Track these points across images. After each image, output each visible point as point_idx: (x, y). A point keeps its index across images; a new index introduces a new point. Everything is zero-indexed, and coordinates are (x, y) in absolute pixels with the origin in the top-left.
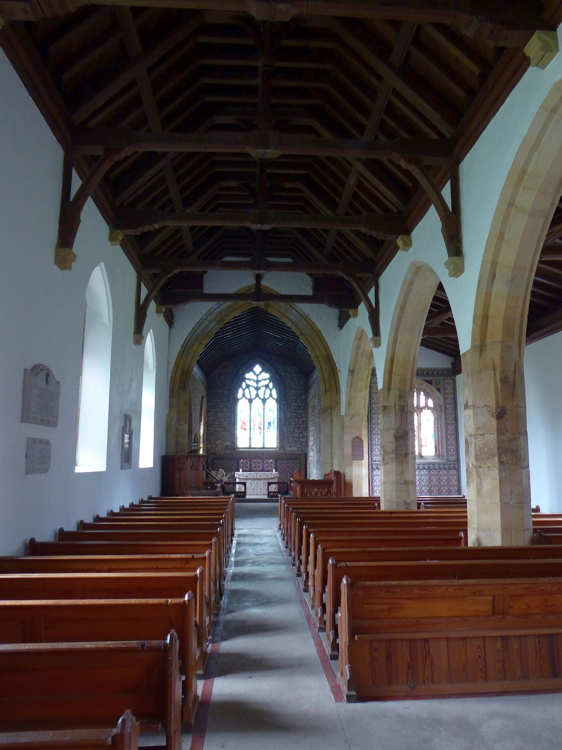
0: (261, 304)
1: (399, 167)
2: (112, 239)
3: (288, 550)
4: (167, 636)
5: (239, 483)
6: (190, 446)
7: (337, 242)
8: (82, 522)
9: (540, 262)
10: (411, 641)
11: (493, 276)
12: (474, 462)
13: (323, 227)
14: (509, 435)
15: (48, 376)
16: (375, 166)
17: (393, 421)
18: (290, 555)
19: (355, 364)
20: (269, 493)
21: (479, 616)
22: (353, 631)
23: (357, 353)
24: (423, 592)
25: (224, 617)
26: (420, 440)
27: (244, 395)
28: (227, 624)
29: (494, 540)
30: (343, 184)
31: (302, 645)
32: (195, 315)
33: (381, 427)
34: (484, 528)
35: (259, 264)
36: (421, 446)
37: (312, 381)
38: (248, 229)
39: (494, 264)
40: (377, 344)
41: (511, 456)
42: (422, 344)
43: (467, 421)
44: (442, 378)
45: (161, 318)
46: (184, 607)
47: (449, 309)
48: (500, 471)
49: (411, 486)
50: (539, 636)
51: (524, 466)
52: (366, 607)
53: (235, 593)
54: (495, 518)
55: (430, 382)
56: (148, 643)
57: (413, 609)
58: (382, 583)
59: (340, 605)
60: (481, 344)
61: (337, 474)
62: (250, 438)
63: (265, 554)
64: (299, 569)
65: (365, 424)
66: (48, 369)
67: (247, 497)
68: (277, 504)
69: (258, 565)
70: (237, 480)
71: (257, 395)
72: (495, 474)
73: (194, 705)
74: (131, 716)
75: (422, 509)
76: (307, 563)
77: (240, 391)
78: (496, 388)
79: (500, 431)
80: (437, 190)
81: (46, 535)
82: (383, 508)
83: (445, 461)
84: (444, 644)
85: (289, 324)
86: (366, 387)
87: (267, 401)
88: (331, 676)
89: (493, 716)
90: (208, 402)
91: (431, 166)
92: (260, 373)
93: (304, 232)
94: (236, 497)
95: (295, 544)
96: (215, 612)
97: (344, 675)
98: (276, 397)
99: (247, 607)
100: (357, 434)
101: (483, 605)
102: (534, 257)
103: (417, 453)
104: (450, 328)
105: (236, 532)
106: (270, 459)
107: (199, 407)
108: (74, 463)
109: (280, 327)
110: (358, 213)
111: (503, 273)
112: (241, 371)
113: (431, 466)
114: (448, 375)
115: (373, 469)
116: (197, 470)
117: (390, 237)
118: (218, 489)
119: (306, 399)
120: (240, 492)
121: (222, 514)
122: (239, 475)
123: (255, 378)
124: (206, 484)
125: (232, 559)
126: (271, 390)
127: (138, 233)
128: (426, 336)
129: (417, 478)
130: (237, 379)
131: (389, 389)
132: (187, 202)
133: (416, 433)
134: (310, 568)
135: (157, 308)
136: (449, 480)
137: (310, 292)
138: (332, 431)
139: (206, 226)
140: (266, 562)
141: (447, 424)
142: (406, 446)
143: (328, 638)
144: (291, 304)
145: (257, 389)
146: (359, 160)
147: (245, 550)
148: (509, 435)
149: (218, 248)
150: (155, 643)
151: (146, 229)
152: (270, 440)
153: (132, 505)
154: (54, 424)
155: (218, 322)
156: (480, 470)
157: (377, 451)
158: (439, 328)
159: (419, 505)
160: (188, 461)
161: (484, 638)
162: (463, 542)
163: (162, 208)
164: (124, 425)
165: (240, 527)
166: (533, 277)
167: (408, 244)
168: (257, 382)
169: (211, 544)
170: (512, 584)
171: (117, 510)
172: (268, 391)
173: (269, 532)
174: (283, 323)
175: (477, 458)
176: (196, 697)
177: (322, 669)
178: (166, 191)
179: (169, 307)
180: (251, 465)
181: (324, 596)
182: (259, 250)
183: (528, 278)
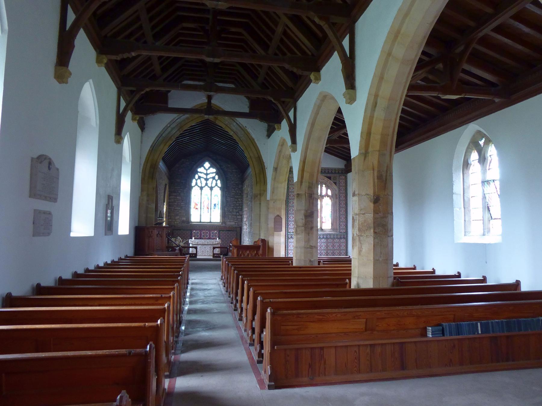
0: (211, 117)
1: (314, 22)
2: (99, 61)
3: (228, 293)
4: (147, 346)
5: (192, 247)
6: (156, 220)
7: (267, 74)
8: (76, 272)
9: (407, 96)
10: (312, 349)
11: (375, 105)
12: (358, 233)
13: (258, 63)
14: (381, 214)
15: (50, 163)
16: (297, 20)
17: (304, 204)
18: (229, 297)
19: (278, 164)
20: (214, 254)
21: (357, 332)
22: (274, 343)
23: (279, 156)
24: (321, 317)
25: (182, 338)
26: (321, 218)
27: (196, 184)
28: (185, 343)
29: (369, 284)
30: (273, 32)
31: (238, 355)
32: (161, 123)
33: (295, 208)
34: (362, 276)
35: (210, 88)
36: (322, 222)
37: (248, 173)
38: (202, 61)
39: (376, 96)
40: (294, 150)
41: (382, 229)
42: (325, 151)
43: (354, 205)
44: (338, 175)
45: (135, 123)
46: (157, 329)
47: (344, 127)
48: (374, 238)
49: (314, 250)
50: (394, 344)
51: (390, 235)
52: (282, 327)
53: (190, 323)
54: (369, 270)
55: (330, 178)
56: (133, 351)
57: (314, 328)
58: (294, 312)
59: (265, 328)
60: (365, 152)
61: (263, 241)
62: (201, 215)
63: (211, 296)
64: (235, 306)
65: (284, 206)
66: (50, 159)
67: (198, 257)
68: (221, 262)
69: (207, 303)
70: (191, 245)
71: (206, 184)
72: (371, 240)
73: (163, 393)
74: (126, 394)
75: (321, 265)
76: (242, 301)
77: (194, 181)
78: (374, 182)
79: (376, 212)
80: (340, 40)
81: (48, 281)
82: (294, 265)
83: (338, 233)
84: (333, 351)
85: (231, 133)
86: (285, 181)
87: (214, 189)
88: (257, 373)
89: (363, 394)
90: (169, 188)
91: (336, 23)
92: (209, 168)
93: (243, 65)
94: (190, 257)
95: (233, 289)
96: (176, 334)
97: (267, 372)
98: (220, 186)
99: (199, 331)
100: (278, 214)
101: (359, 324)
102: (403, 92)
103: (319, 227)
104: (345, 140)
105: (190, 282)
106: (215, 230)
107: (163, 191)
108: (69, 231)
109: (224, 135)
110: (284, 54)
111: (382, 103)
112: (195, 166)
113: (328, 237)
114: (342, 173)
115: (288, 238)
116: (161, 237)
117: (305, 73)
118: (177, 251)
119: (242, 188)
120: (193, 254)
121: (181, 268)
122: (192, 241)
123: (205, 172)
124: (168, 248)
125: (187, 300)
126: (216, 181)
127: (119, 59)
128: (328, 145)
129: (319, 244)
130: (191, 172)
131: (301, 182)
132: (157, 36)
133: (319, 214)
134: (244, 305)
135: (132, 117)
136: (340, 246)
137: (246, 110)
138: (260, 211)
139: (170, 57)
140: (212, 301)
141: (340, 207)
142: (312, 222)
143: (256, 350)
144: (233, 118)
145: (207, 179)
146: (286, 15)
147: (197, 294)
148: (381, 214)
149: (180, 73)
150: (138, 350)
151: (126, 56)
152: (214, 216)
153: (113, 261)
154: (55, 200)
155: (179, 130)
156: (361, 238)
157: (292, 225)
158: (337, 139)
159: (319, 262)
160: (155, 231)
161: (359, 346)
162: (348, 285)
163: (137, 40)
164: (107, 203)
165: (193, 278)
166: (401, 106)
167: (318, 79)
168: (207, 174)
169: (174, 288)
170: (379, 311)
171: (102, 265)
172: (214, 181)
173: (214, 281)
174: (227, 132)
175: (360, 230)
176: (164, 389)
177: (251, 370)
178: (141, 27)
179: (143, 116)
180: (201, 234)
181: (254, 323)
182: (210, 77)
183: (398, 107)
